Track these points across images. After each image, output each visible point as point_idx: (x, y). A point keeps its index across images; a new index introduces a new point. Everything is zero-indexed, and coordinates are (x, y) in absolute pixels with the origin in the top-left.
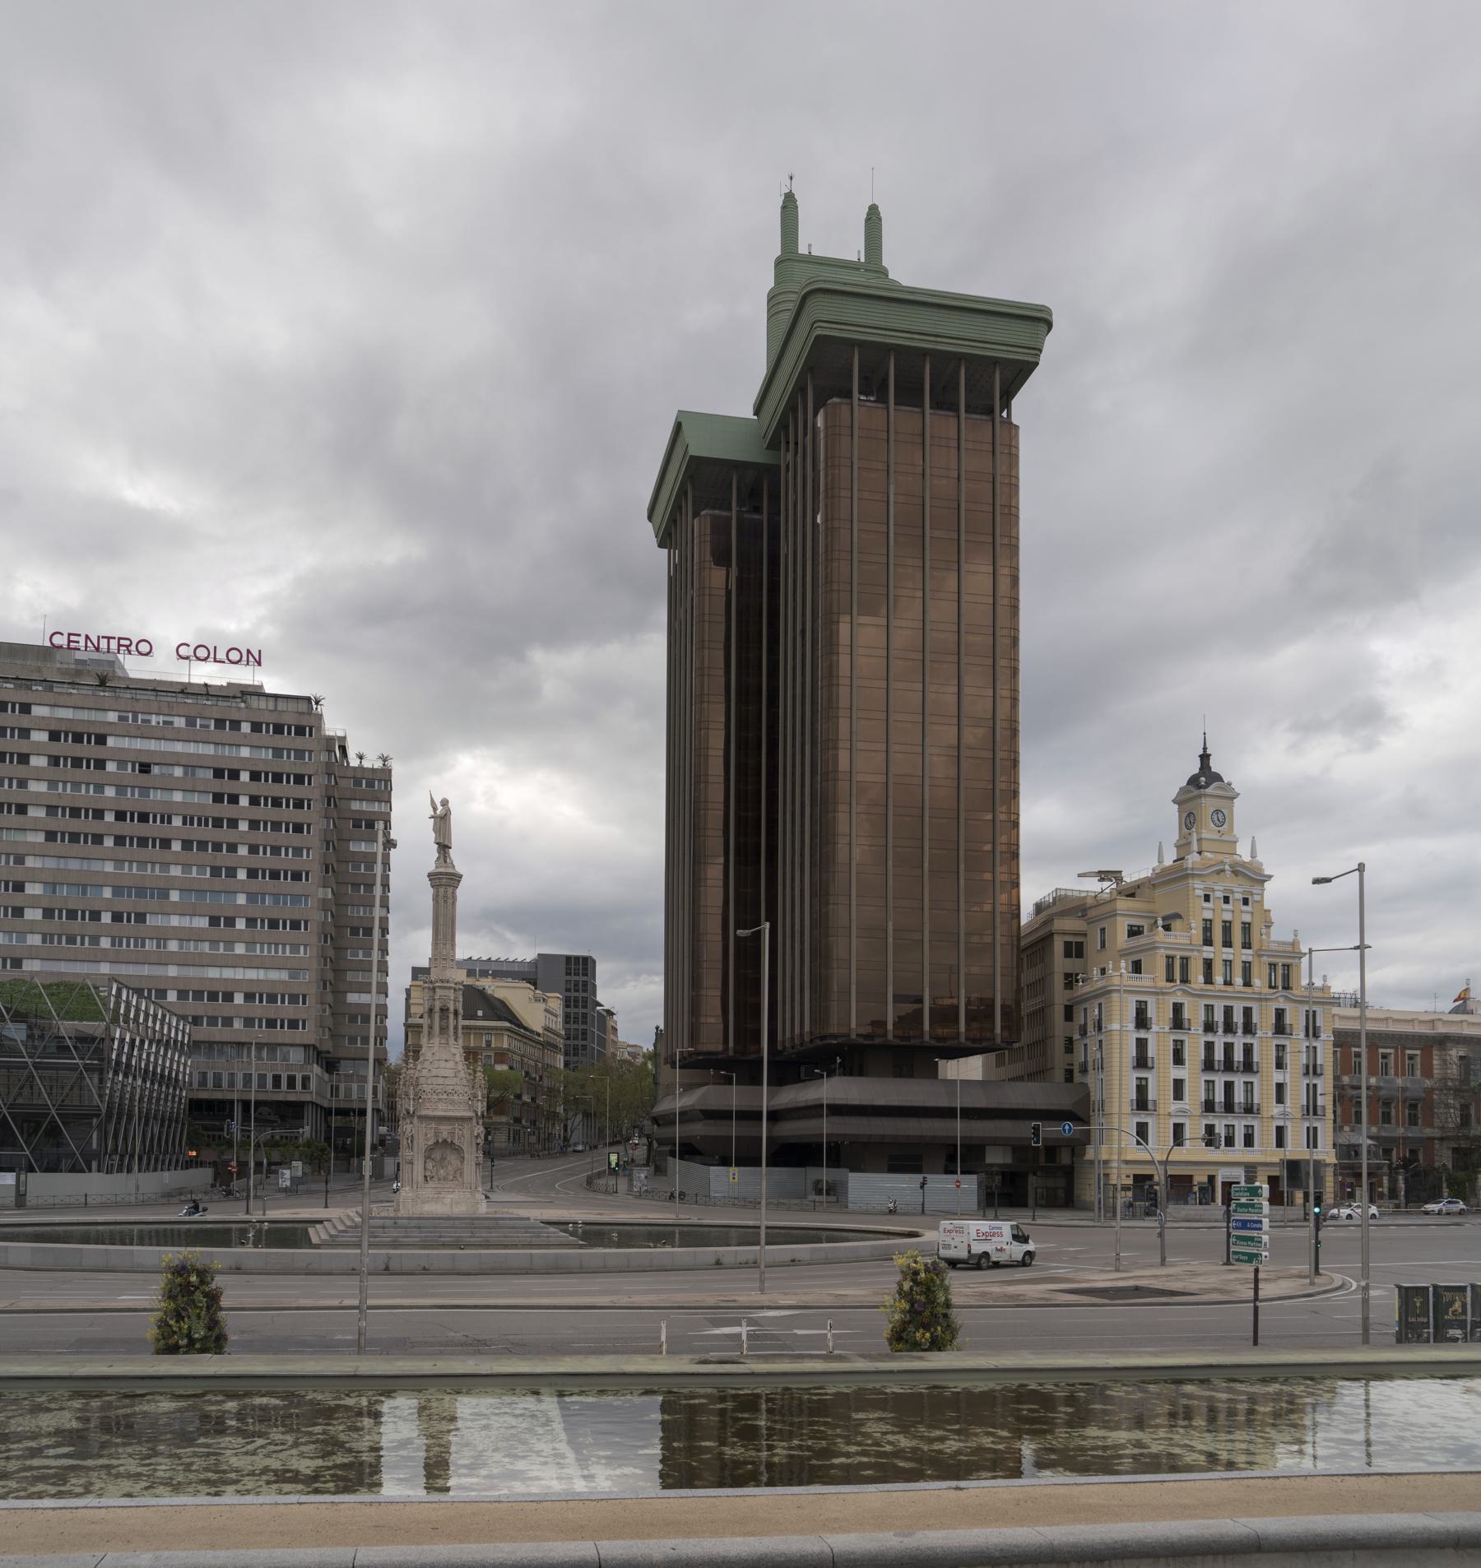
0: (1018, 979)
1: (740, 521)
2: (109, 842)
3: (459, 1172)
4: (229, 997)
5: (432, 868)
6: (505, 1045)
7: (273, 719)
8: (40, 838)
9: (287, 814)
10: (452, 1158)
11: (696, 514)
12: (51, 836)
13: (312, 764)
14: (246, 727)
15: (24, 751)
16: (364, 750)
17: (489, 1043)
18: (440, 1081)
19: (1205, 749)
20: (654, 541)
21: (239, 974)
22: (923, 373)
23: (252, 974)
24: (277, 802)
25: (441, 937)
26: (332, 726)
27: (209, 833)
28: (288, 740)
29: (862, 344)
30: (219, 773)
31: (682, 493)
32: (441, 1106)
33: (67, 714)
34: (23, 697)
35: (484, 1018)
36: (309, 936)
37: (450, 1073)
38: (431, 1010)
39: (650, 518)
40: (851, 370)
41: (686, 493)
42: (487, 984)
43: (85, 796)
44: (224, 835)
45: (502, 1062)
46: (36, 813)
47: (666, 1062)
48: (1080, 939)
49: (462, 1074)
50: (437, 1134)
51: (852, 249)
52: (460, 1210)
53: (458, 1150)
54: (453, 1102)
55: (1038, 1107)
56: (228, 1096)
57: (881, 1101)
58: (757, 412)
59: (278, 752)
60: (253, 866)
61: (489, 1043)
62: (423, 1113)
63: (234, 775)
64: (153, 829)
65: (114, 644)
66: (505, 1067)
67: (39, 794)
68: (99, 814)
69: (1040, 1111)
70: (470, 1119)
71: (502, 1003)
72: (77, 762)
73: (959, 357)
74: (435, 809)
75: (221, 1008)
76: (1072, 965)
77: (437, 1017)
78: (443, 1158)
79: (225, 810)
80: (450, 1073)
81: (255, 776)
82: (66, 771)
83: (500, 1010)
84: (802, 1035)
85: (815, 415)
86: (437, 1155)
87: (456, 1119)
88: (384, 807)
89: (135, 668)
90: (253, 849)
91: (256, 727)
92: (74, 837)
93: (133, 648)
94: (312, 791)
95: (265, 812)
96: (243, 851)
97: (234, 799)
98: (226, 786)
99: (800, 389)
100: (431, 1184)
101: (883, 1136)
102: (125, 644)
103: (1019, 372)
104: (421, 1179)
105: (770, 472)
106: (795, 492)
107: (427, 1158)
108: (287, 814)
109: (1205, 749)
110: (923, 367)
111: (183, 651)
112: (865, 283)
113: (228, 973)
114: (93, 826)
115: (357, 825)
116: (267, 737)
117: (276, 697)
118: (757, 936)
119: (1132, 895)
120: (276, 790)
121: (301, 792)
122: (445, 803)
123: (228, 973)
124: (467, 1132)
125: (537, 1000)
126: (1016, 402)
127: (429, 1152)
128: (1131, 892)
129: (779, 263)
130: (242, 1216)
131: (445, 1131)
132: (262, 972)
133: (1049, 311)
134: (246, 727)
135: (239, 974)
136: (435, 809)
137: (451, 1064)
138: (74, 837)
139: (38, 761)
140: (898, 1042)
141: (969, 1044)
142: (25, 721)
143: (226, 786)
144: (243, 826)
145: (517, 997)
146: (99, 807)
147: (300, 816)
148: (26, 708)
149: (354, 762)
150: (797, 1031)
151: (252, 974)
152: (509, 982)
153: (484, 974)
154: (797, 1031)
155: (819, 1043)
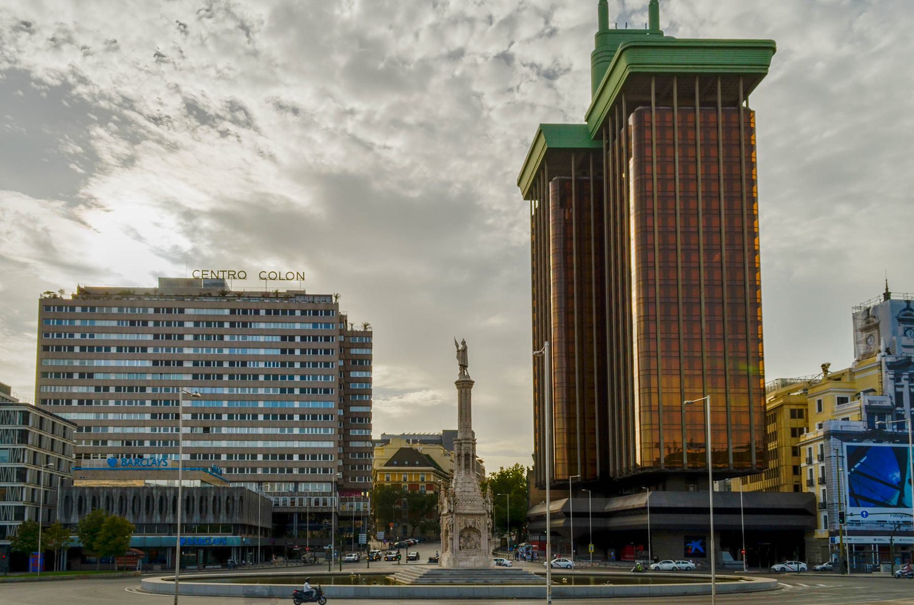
0: (766, 431)
2: (226, 378)
4: (290, 457)
5: (457, 378)
6: (432, 480)
7: (243, 306)
8: (189, 377)
10: (474, 536)
11: (550, 180)
12: (195, 376)
13: (333, 329)
14: (298, 313)
16: (355, 323)
17: (423, 480)
19: (887, 289)
20: (522, 197)
21: (296, 444)
22: (694, 88)
23: (303, 444)
24: (315, 352)
25: (463, 415)
26: (342, 310)
27: (279, 370)
28: (321, 318)
30: (283, 338)
31: (541, 167)
34: (180, 304)
35: (420, 465)
36: (334, 421)
39: (519, 184)
40: (694, 94)
41: (543, 169)
42: (418, 447)
43: (174, 354)
44: (287, 370)
45: (430, 489)
46: (188, 364)
47: (536, 486)
48: (800, 407)
49: (478, 491)
50: (465, 524)
51: (641, 22)
52: (480, 565)
53: (478, 532)
54: (474, 506)
55: (767, 507)
58: (587, 120)
59: (315, 325)
61: (423, 480)
63: (292, 338)
65: (226, 274)
66: (432, 492)
68: (220, 364)
69: (727, 513)
70: (484, 514)
71: (428, 456)
72: (169, 337)
75: (286, 462)
77: (463, 459)
78: (469, 537)
79: (288, 357)
81: (303, 339)
82: (162, 341)
83: (427, 461)
84: (621, 470)
85: (628, 117)
86: (466, 534)
87: (477, 514)
88: (368, 352)
89: (234, 286)
90: (303, 378)
91: (303, 313)
92: (208, 377)
93: (236, 276)
94: (334, 345)
95: (309, 357)
96: (297, 378)
97: (292, 351)
98: (288, 344)
99: (617, 102)
100: (463, 551)
101: (669, 525)
102: (233, 275)
103: (753, 79)
104: (457, 548)
105: (597, 153)
108: (321, 357)
109: (887, 289)
110: (695, 84)
111: (263, 275)
112: (650, 41)
113: (290, 444)
114: (218, 370)
115: (354, 363)
119: (839, 379)
120: (314, 345)
121: (327, 358)
123: (290, 444)
126: (750, 97)
130: (326, 572)
131: (470, 521)
133: (773, 42)
134: (298, 313)
135: (296, 444)
137: (470, 485)
138: (208, 377)
139: (189, 338)
141: (736, 471)
142: (181, 317)
143: (288, 344)
145: (436, 453)
146: (220, 359)
147: (327, 358)
148: (182, 311)
149: (349, 329)
151: (303, 444)
152: (433, 446)
155: (640, 472)
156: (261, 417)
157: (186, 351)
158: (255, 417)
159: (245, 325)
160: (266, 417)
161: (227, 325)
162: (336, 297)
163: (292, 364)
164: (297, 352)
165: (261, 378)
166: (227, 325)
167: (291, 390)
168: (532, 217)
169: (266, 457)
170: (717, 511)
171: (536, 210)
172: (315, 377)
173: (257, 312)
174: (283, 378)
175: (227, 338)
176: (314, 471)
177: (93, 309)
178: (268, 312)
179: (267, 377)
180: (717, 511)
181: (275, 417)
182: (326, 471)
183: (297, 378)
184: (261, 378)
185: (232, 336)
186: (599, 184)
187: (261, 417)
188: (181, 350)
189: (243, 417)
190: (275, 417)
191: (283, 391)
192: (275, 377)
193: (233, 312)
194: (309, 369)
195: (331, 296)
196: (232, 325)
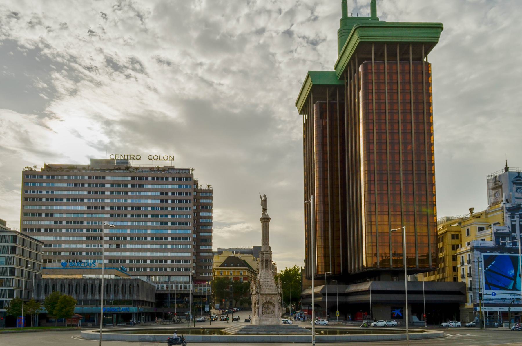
0: (437, 246)
1: (329, 103)
2: (129, 216)
3: (272, 312)
4: (166, 261)
5: (261, 216)
8: (108, 216)
9: (183, 204)
10: (271, 307)
11: (314, 103)
12: (112, 215)
13: (190, 188)
14: (170, 179)
15: (103, 190)
16: (203, 185)
17: (241, 274)
18: (266, 282)
19: (507, 165)
21: (169, 254)
24: (180, 201)
27: (159, 212)
28: (183, 182)
29: (375, 43)
30: (162, 194)
31: (309, 96)
32: (267, 290)
33: (117, 178)
34: (103, 174)
35: (240, 266)
37: (269, 280)
38: (262, 260)
39: (296, 105)
40: (397, 54)
42: (239, 256)
43: (99, 202)
44: (164, 212)
46: (107, 208)
48: (457, 233)
49: (273, 281)
51: (366, 12)
52: (274, 323)
53: (273, 304)
56: (167, 292)
57: (389, 289)
58: (335, 68)
59: (180, 186)
60: (173, 221)
61: (241, 274)
62: (262, 293)
63: (167, 194)
64: (122, 211)
66: (246, 282)
67: (108, 203)
68: (126, 208)
70: (277, 294)
71: (244, 261)
73: (409, 43)
74: (261, 198)
76: (456, 242)
78: (268, 307)
79: (164, 204)
80: (269, 280)
81: (173, 194)
83: (244, 264)
86: (266, 306)
87: (272, 294)
88: (210, 201)
89: (134, 164)
90: (173, 216)
91: (173, 179)
93: (135, 158)
94: (191, 197)
95: (177, 204)
96: (170, 216)
97: (167, 201)
98: (164, 197)
99: (353, 58)
100: (264, 315)
103: (430, 45)
104: (261, 313)
105: (341, 88)
106: (351, 90)
107: (263, 307)
108: (183, 204)
109: (507, 165)
111: (150, 158)
112: (371, 23)
114: (125, 212)
115: (202, 207)
116: (177, 181)
117: (179, 169)
118: (402, 230)
119: (479, 217)
120: (179, 197)
121: (187, 205)
122: (265, 196)
123: (165, 254)
124: (275, 298)
125: (254, 260)
126: (429, 55)
127: (264, 304)
128: (478, 216)
129: (341, 20)
130: (186, 327)
131: (268, 298)
132: (176, 253)
133: (441, 24)
134: (170, 179)
135: (169, 254)
136: (261, 198)
138: (119, 215)
139: (108, 193)
140: (381, 269)
141: (420, 269)
142: (103, 181)
143: (164, 197)
144: (170, 209)
145: (249, 259)
146: (126, 206)
147: (187, 205)
148: (104, 178)
149: (199, 188)
150: (357, 266)
151: (173, 254)
153: (237, 253)
154: (357, 266)
155: (365, 270)
156: (149, 239)
157: (107, 201)
158: (146, 238)
159: (140, 186)
160: (152, 238)
161: (129, 186)
162: (192, 170)
163: (167, 208)
164: (170, 201)
165: (149, 216)
166: (129, 186)
167: (166, 223)
168: (304, 124)
169: (152, 261)
170: (409, 292)
171: (306, 120)
172: (180, 216)
173: (147, 178)
174: (162, 216)
175: (129, 193)
176: (179, 269)
177: (53, 177)
178: (153, 179)
179: (152, 216)
180: (409, 292)
181: (157, 238)
182: (186, 269)
183: (170, 216)
184: (149, 216)
185: (133, 192)
186: (342, 105)
187: (149, 239)
188: (103, 200)
189: (139, 238)
190: (157, 238)
191: (161, 223)
192: (157, 216)
193: (133, 178)
194: (176, 211)
195: (189, 169)
196: (133, 186)
